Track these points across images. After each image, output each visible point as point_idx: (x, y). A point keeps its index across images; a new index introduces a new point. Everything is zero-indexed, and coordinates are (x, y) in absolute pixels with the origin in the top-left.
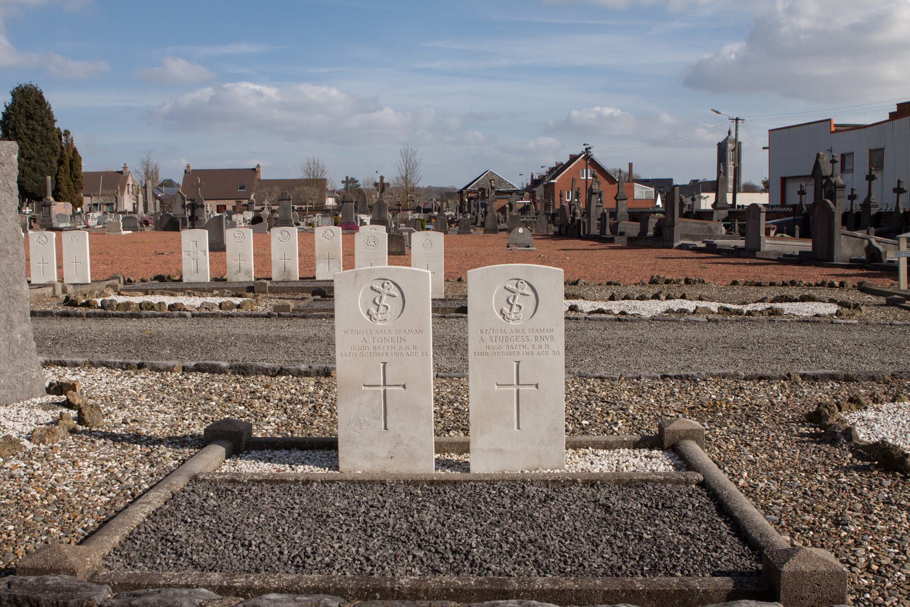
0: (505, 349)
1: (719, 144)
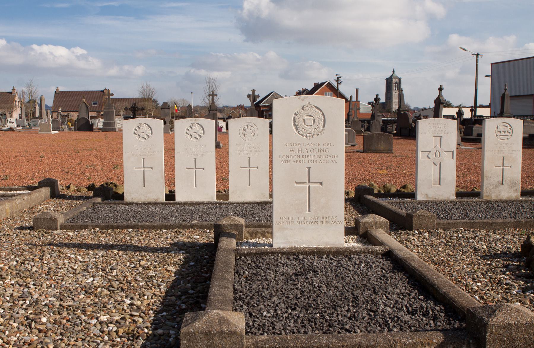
0: (308, 220)
1: (387, 79)
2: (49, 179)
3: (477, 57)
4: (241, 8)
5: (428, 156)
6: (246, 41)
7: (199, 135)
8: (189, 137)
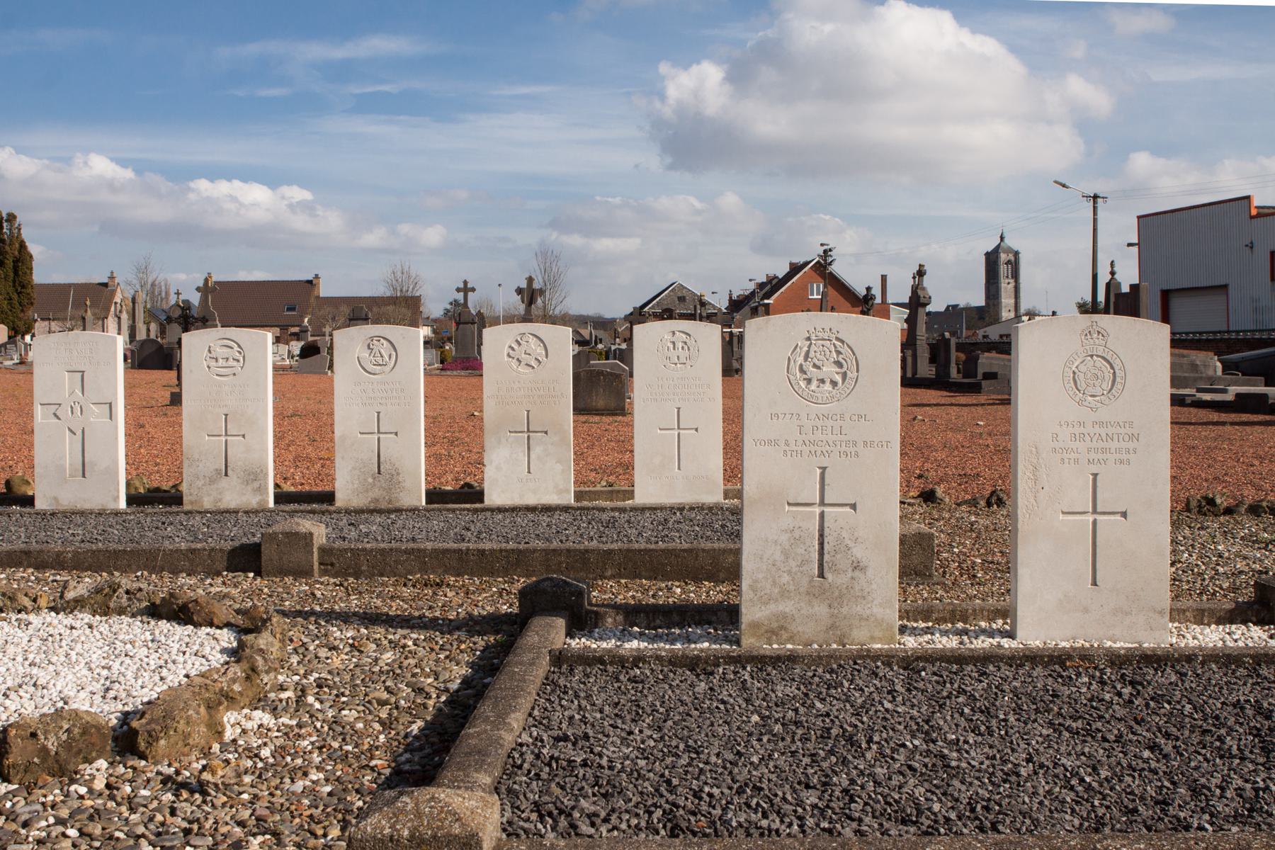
1: (987, 254)
3: (1095, 203)
4: (662, 97)
5: (55, 415)
6: (671, 167)
8: (514, 363)
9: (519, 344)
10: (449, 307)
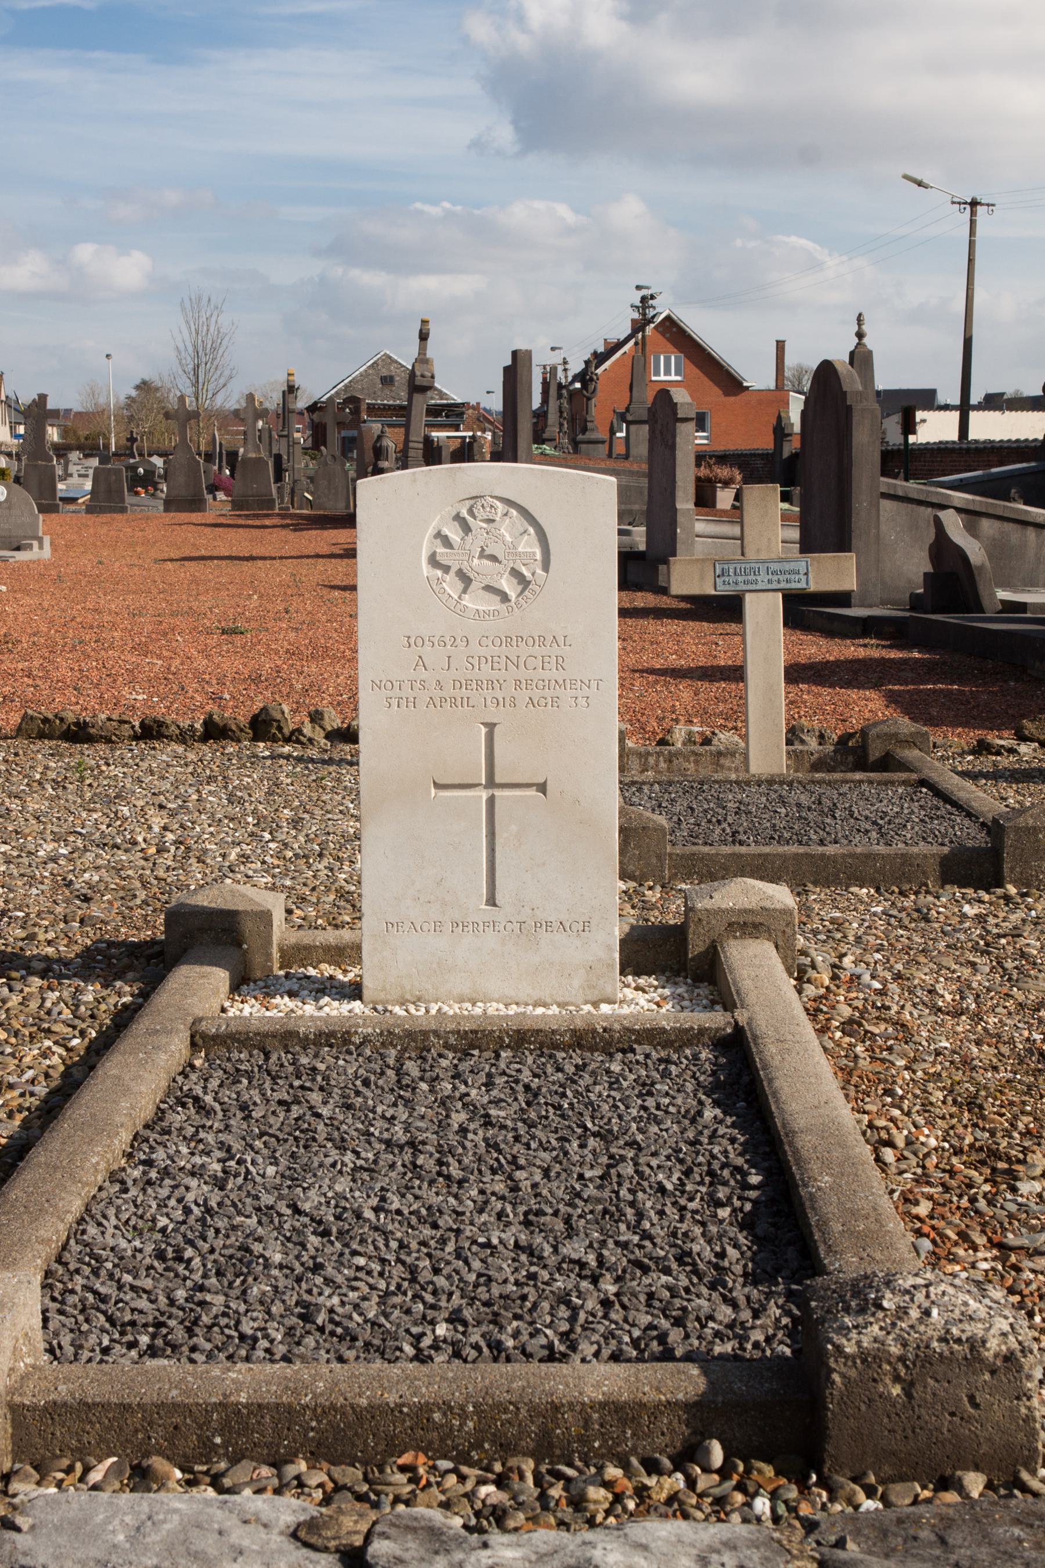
2: (623, 942)
3: (973, 213)
7: (515, 573)
8: (451, 585)
9: (466, 529)
10: (134, 393)
